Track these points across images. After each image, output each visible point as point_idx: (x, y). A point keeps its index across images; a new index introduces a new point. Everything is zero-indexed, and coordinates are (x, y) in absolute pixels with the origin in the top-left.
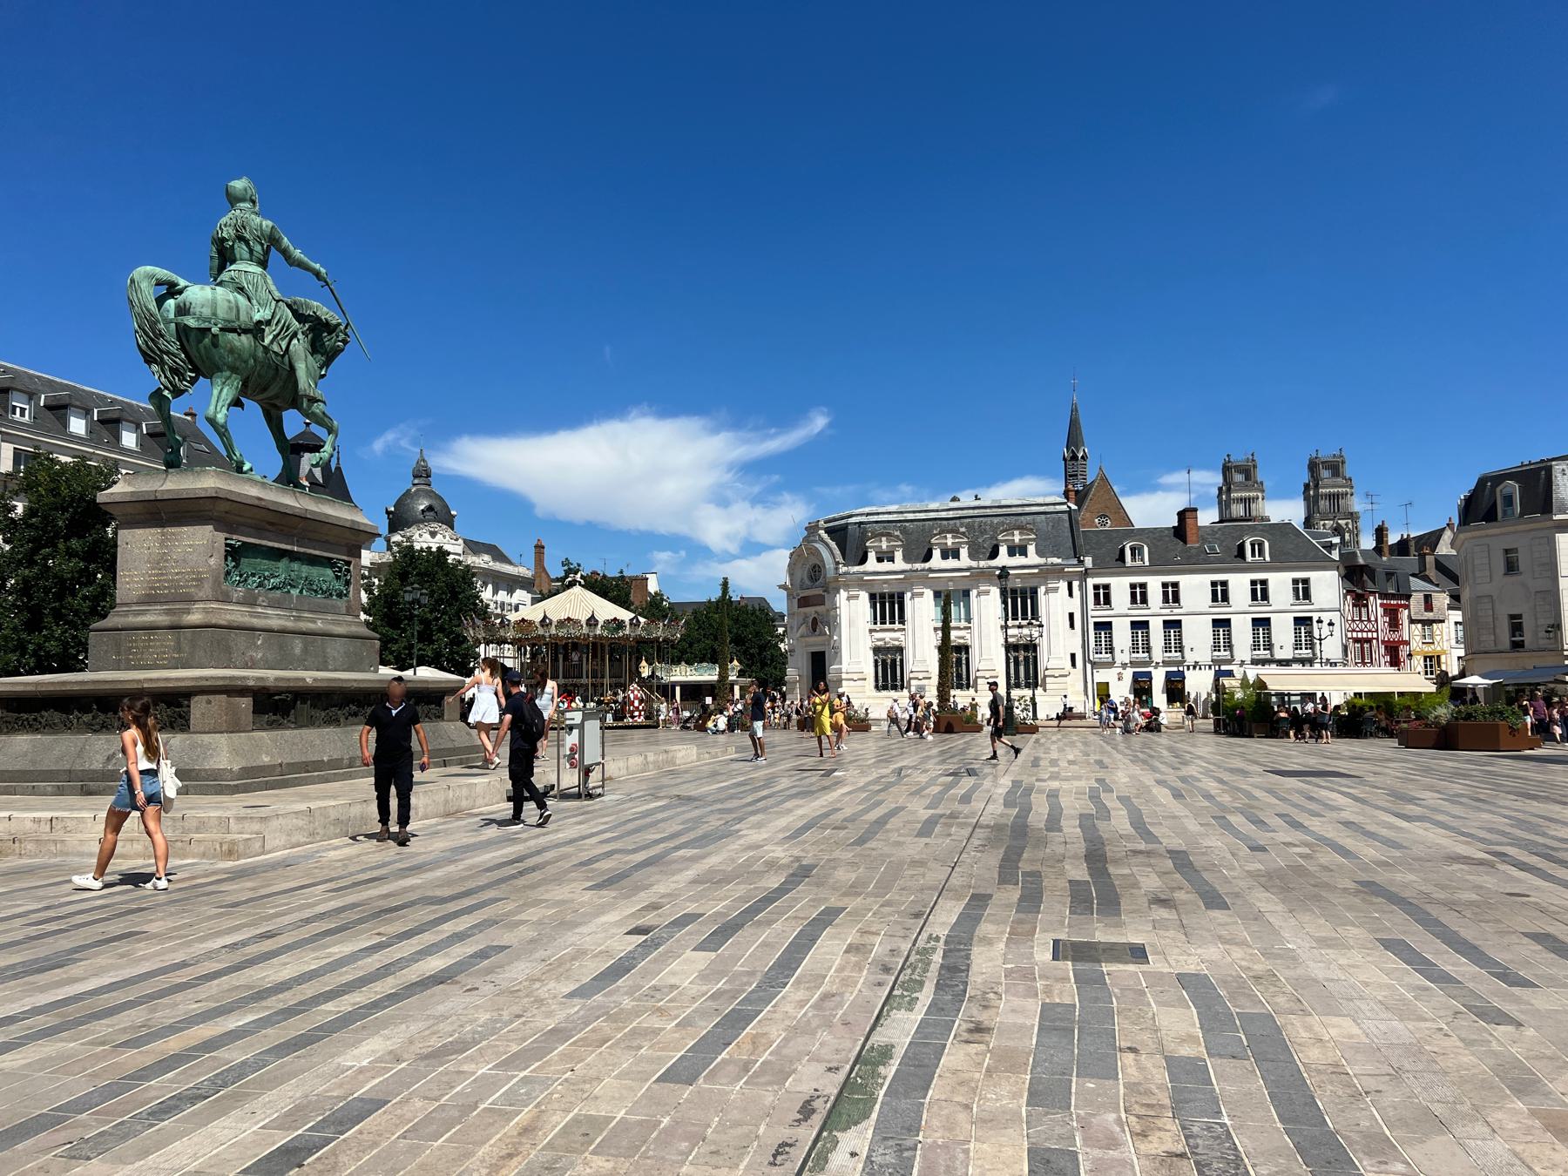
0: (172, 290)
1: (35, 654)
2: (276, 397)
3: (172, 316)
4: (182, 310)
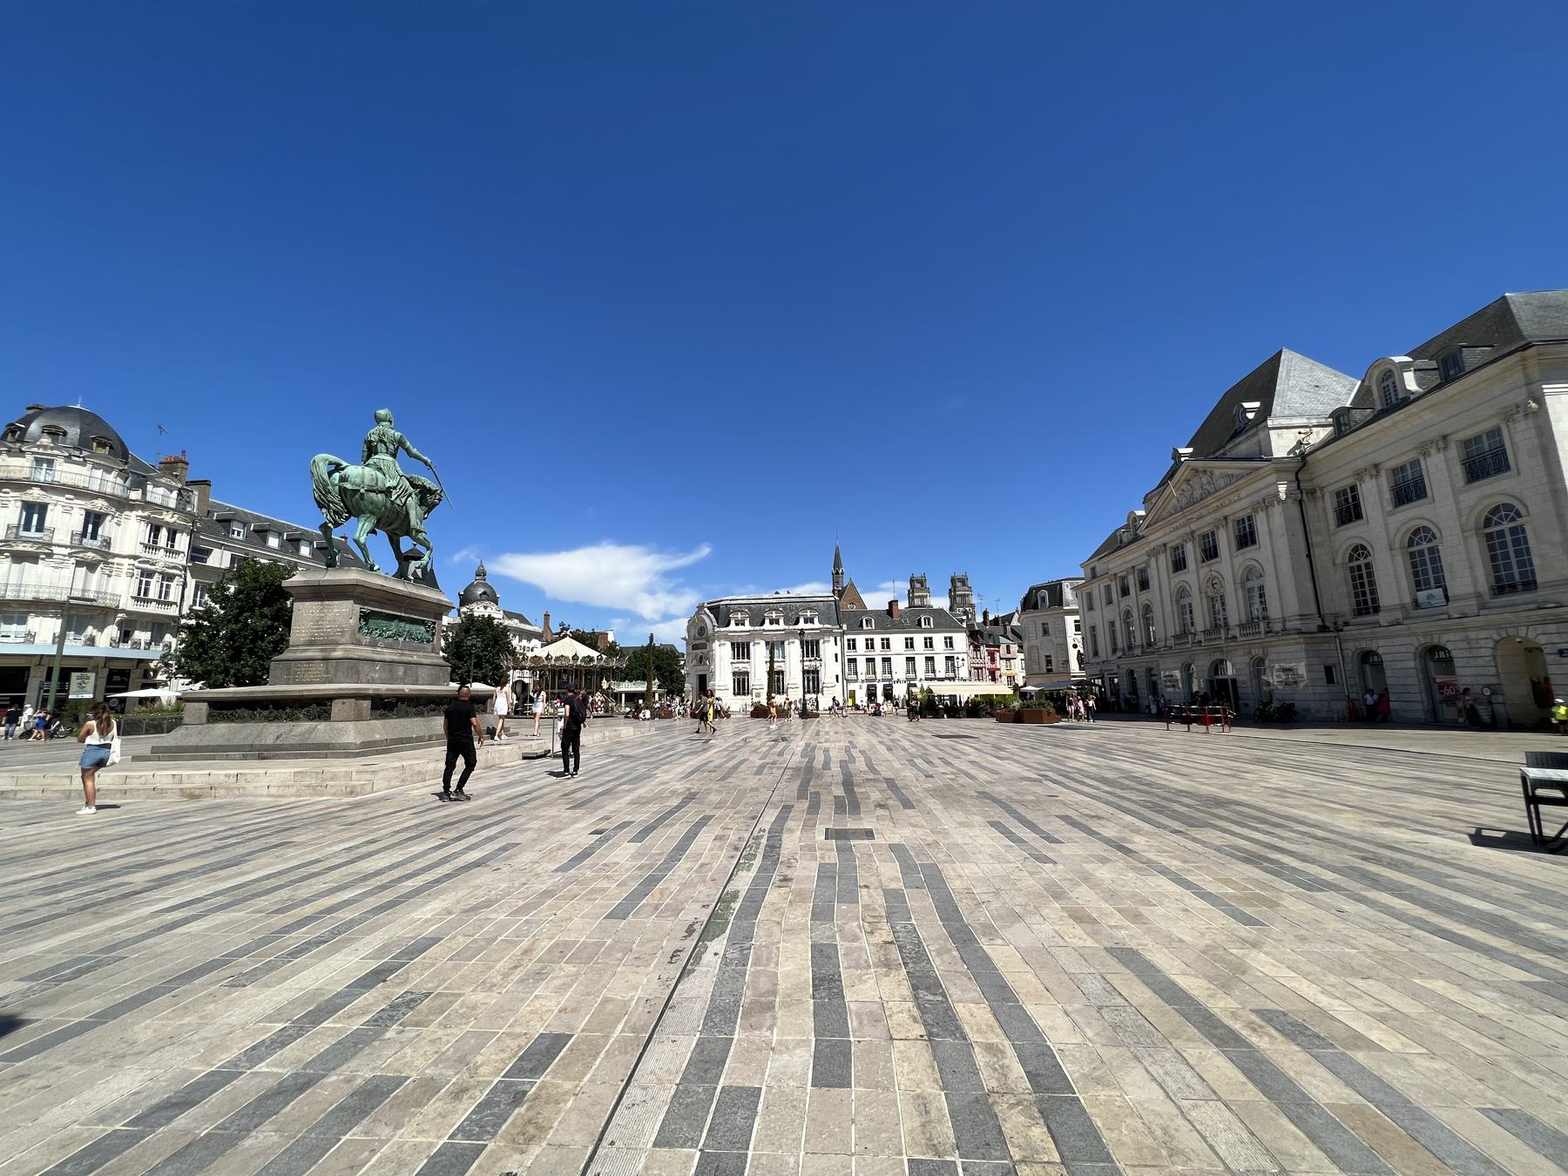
4: (343, 479)
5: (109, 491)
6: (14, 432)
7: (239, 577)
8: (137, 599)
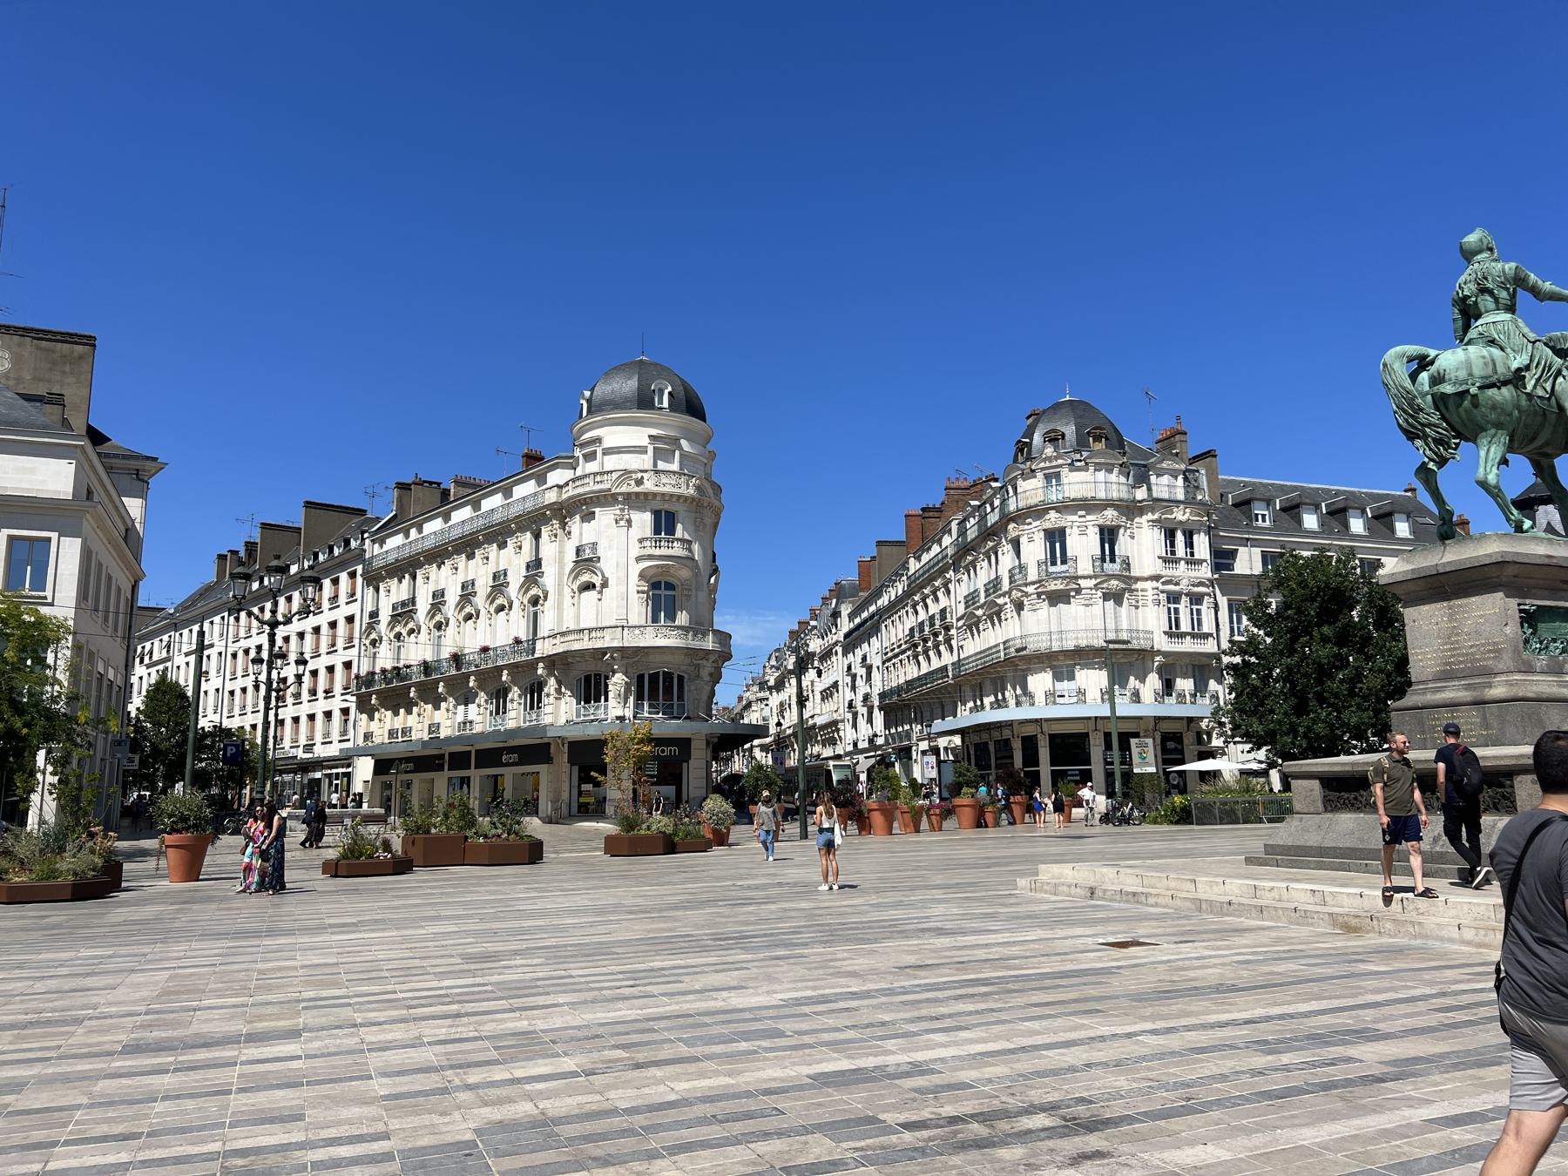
0: (1423, 363)
1: (1305, 736)
2: (1547, 444)
3: (1427, 388)
4: (1437, 380)
5: (1115, 495)
6: (1022, 451)
7: (1279, 584)
8: (1170, 634)
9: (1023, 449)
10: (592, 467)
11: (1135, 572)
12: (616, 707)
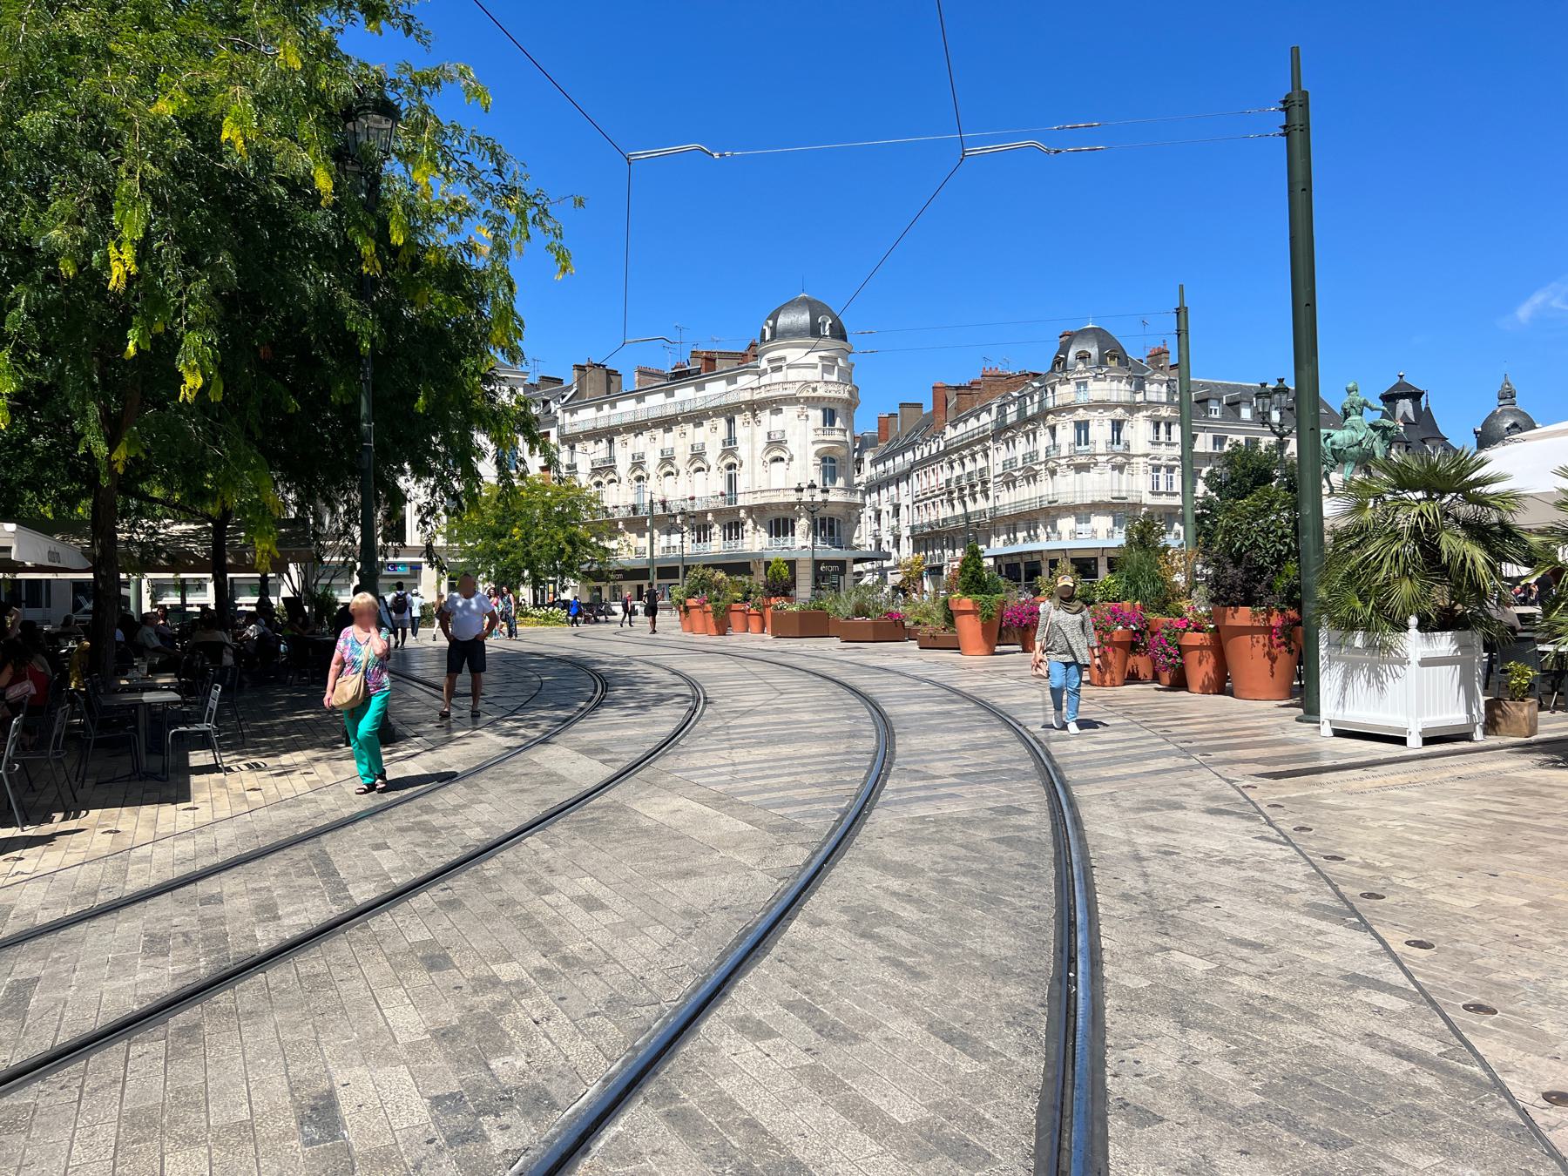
4: (1333, 443)
5: (1123, 399)
8: (1153, 493)
9: (1060, 363)
10: (778, 377)
11: (1132, 451)
12: (801, 540)
